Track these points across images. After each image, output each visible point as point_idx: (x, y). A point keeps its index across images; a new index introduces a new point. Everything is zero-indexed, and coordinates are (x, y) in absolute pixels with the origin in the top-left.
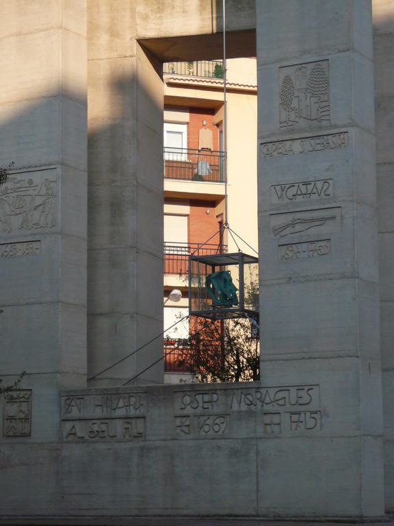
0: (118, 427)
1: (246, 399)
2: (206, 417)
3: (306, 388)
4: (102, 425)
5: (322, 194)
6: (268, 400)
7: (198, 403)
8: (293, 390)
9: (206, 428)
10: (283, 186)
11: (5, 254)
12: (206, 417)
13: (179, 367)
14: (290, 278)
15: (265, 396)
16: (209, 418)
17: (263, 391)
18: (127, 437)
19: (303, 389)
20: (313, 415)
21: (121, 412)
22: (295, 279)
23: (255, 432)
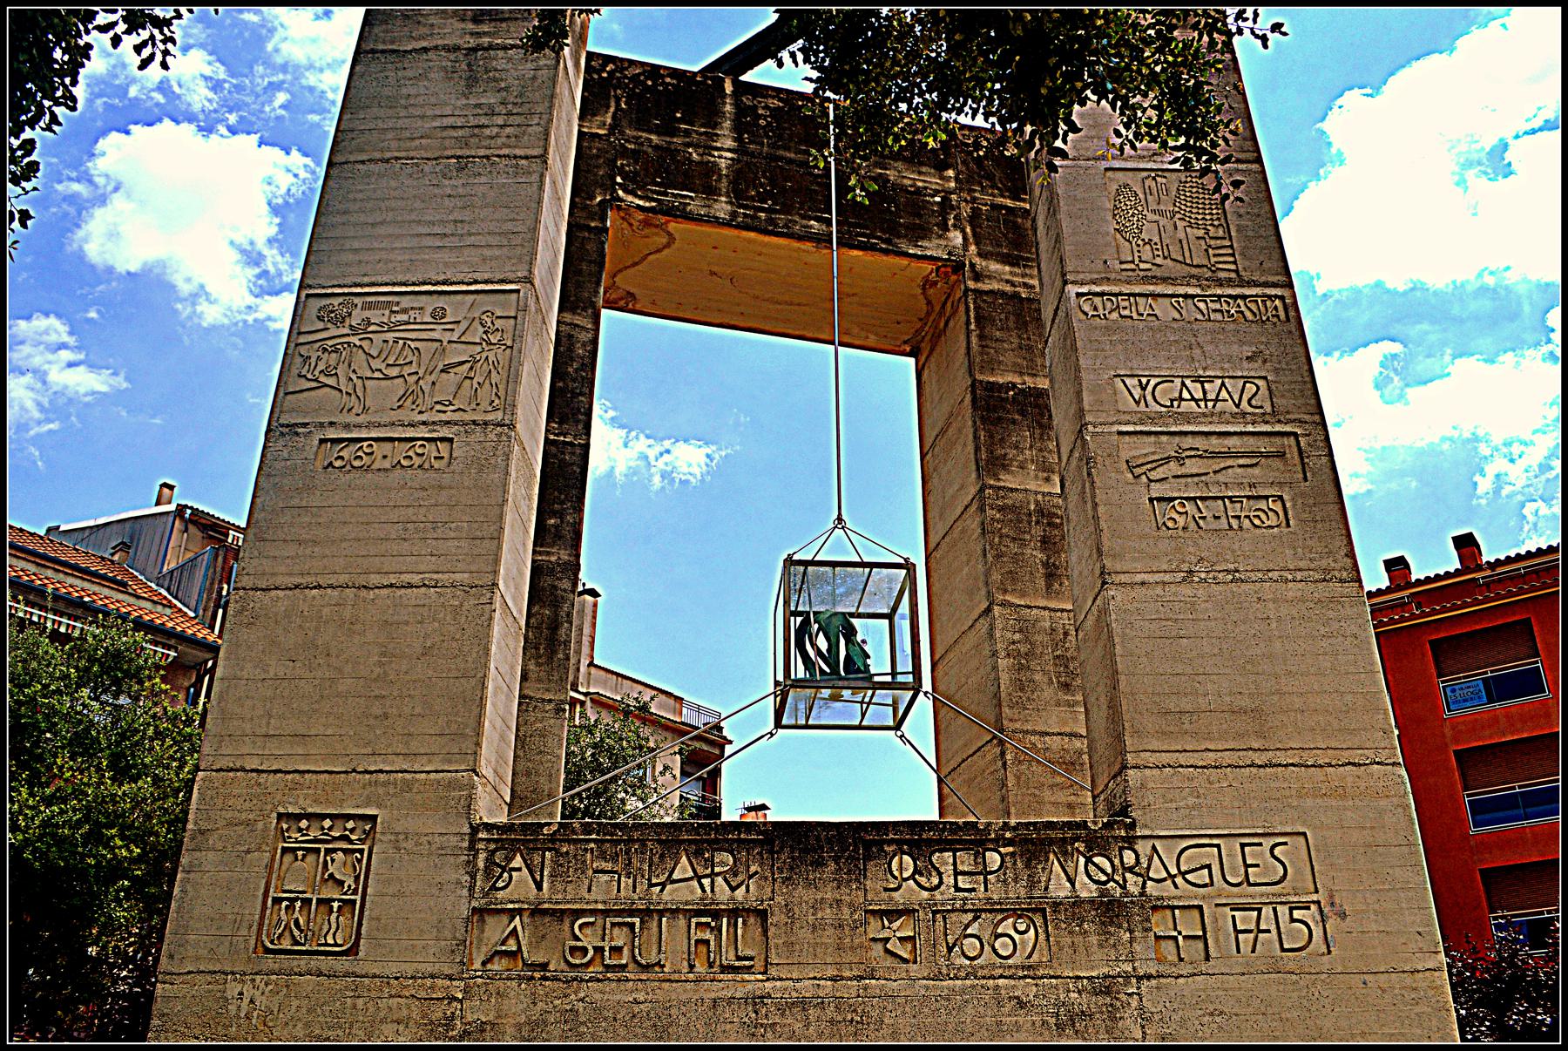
0: (675, 938)
1: (1091, 868)
2: (970, 916)
3: (1268, 843)
4: (616, 931)
5: (1244, 404)
6: (1157, 872)
7: (940, 874)
8: (1231, 848)
9: (971, 946)
10: (1144, 380)
11: (338, 463)
12: (970, 916)
13: (1052, 842)
14: (1190, 572)
15: (1150, 860)
16: (975, 919)
17: (1143, 847)
18: (700, 968)
19: (1260, 844)
20: (1296, 914)
21: (689, 893)
22: (1203, 575)
23: (1071, 765)
